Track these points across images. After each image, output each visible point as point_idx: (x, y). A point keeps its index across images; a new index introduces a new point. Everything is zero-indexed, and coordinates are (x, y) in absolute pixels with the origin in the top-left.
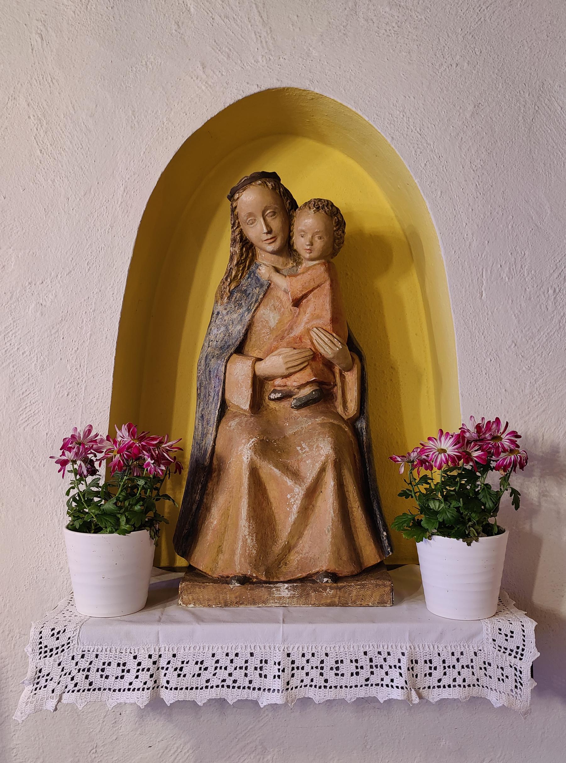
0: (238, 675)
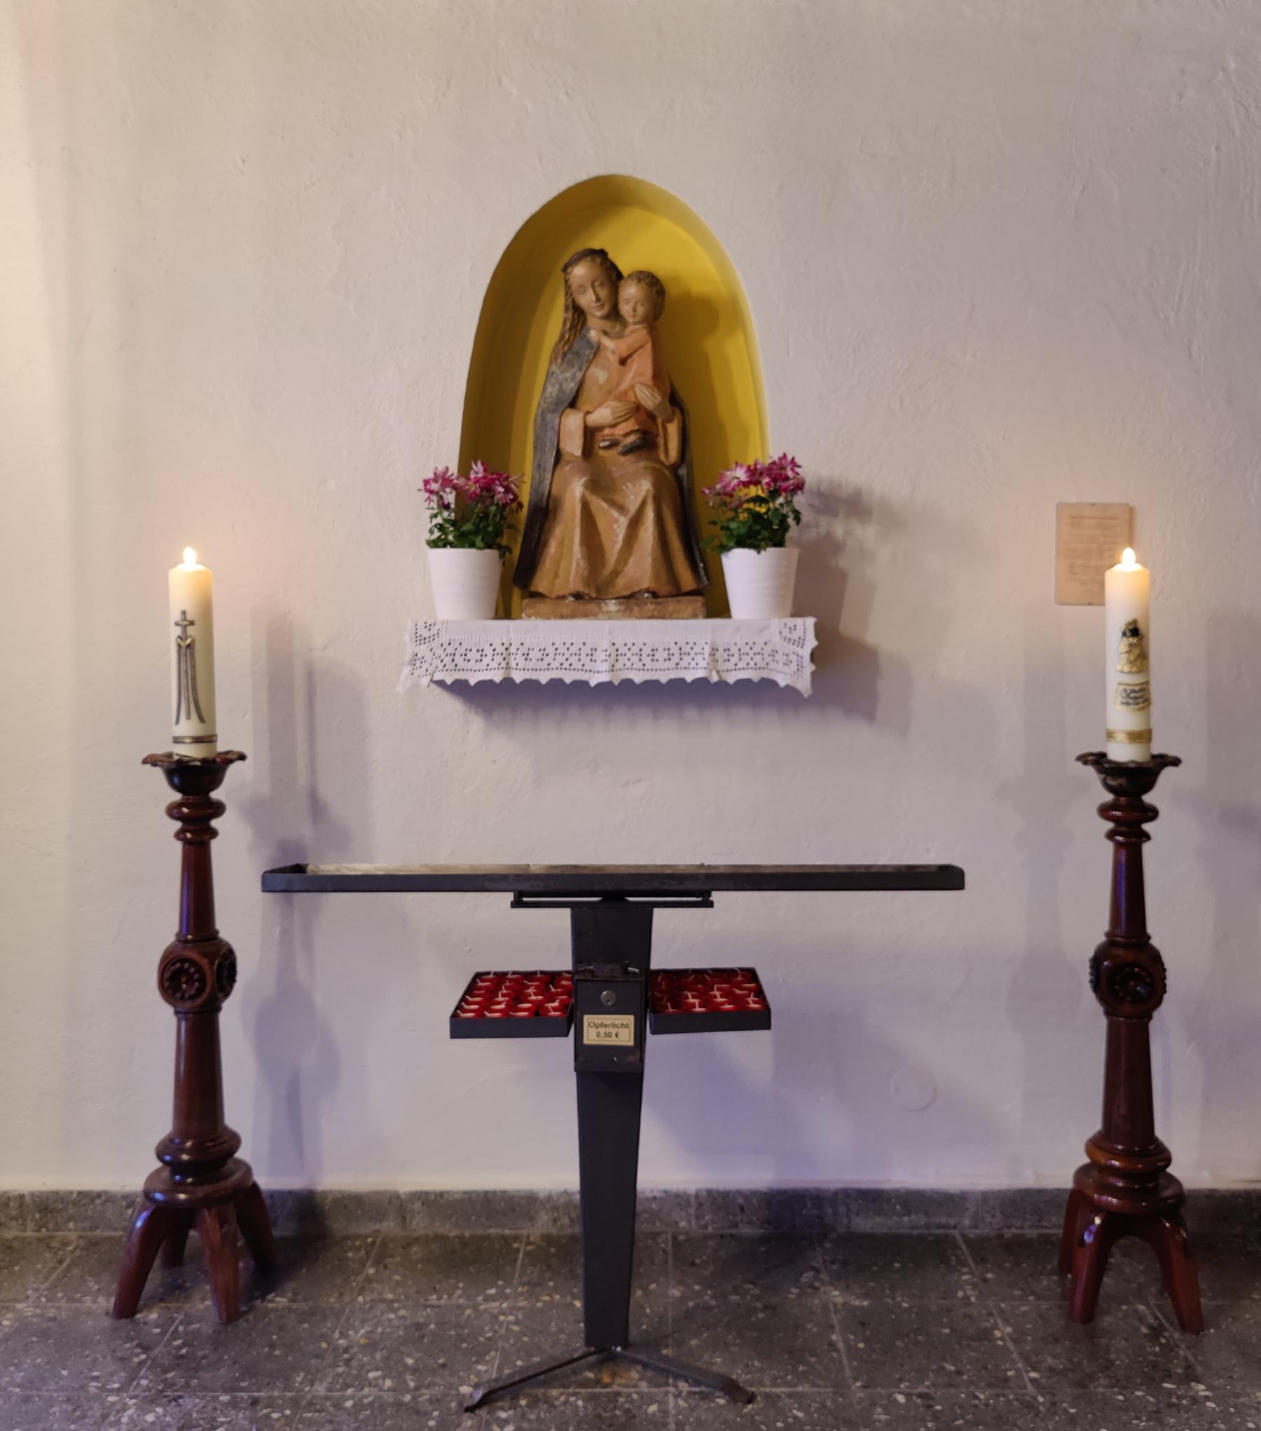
0: (573, 659)
